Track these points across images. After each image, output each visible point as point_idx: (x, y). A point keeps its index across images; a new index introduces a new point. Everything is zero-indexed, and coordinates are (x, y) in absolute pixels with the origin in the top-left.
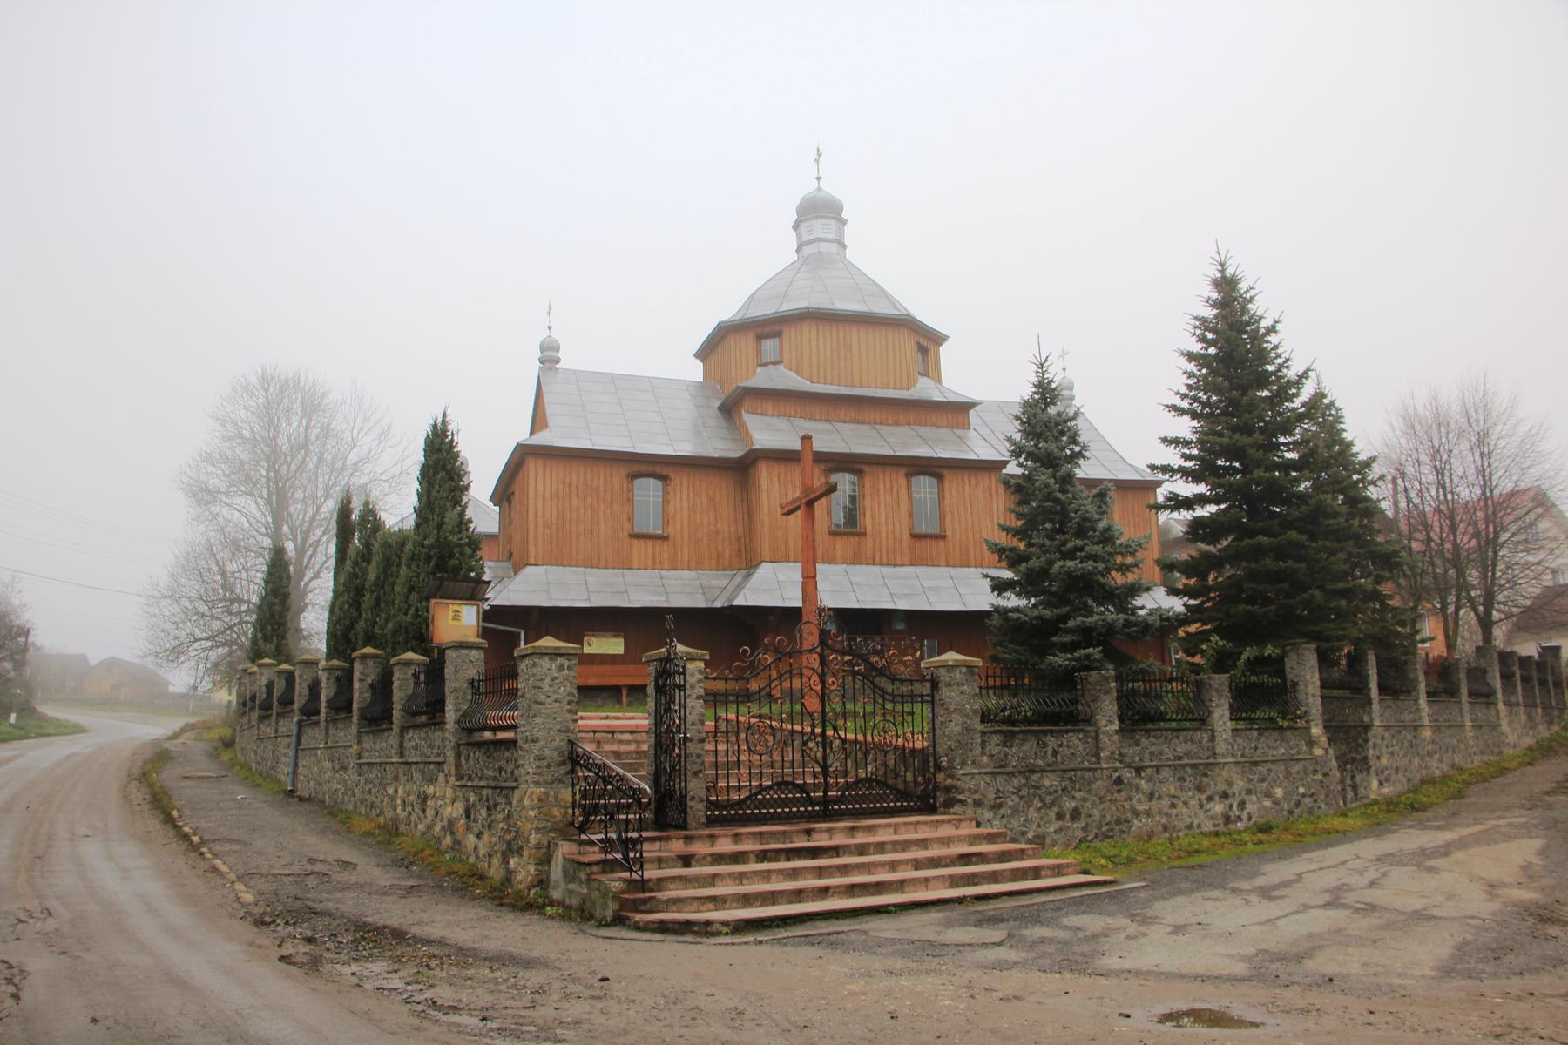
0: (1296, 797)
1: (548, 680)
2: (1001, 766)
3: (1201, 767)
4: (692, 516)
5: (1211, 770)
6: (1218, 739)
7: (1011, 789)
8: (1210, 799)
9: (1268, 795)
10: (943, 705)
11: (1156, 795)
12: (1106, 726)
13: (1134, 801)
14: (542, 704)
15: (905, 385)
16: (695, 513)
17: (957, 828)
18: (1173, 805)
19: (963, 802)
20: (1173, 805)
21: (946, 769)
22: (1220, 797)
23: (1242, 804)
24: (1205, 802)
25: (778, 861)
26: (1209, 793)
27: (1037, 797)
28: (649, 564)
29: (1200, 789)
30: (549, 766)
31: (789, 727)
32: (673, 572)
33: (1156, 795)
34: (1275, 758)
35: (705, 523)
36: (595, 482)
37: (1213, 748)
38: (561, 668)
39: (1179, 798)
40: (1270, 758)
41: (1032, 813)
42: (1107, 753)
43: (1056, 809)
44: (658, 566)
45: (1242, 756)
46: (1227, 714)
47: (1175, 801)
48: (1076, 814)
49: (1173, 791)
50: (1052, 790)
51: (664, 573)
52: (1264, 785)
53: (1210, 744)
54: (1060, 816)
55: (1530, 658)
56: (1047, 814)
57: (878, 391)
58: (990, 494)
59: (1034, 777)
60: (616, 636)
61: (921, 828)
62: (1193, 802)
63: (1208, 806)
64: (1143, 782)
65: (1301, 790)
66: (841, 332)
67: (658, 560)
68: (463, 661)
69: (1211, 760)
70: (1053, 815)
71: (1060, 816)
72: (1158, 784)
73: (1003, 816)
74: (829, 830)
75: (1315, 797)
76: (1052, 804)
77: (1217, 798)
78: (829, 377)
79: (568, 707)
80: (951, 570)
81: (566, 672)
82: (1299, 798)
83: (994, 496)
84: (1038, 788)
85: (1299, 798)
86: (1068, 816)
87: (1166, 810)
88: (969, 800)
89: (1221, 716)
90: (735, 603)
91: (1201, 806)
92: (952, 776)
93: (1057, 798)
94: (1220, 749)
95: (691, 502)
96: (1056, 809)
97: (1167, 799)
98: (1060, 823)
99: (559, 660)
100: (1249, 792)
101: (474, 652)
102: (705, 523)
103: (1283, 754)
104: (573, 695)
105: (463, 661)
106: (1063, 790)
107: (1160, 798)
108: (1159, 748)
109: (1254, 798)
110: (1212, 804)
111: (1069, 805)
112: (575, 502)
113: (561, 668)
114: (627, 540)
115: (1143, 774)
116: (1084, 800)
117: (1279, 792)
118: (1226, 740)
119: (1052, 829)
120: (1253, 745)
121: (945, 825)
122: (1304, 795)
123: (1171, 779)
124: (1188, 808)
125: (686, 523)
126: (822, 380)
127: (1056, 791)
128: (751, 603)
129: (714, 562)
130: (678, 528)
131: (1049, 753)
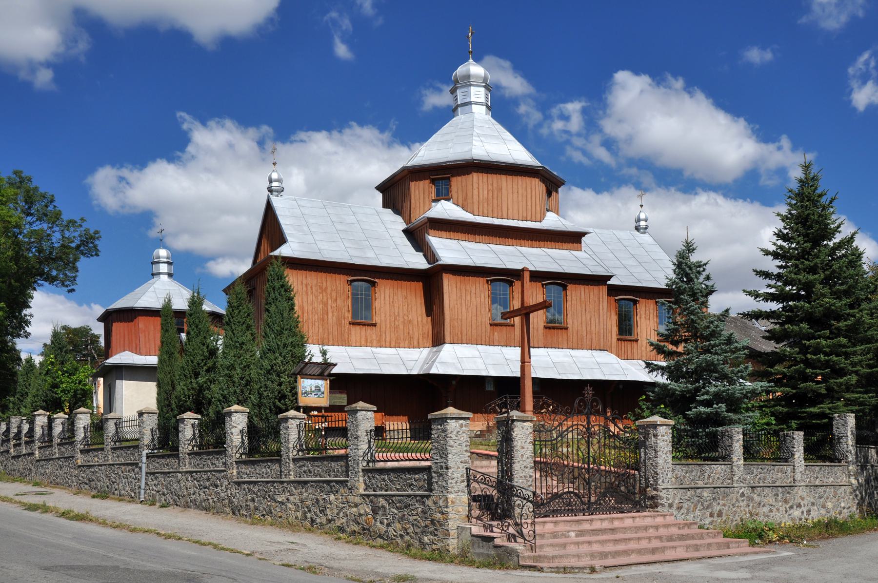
0: (839, 509)
1: (455, 433)
2: (682, 484)
3: (787, 488)
4: (392, 310)
5: (792, 490)
6: (797, 471)
7: (687, 498)
8: (791, 507)
9: (824, 507)
10: (652, 447)
11: (762, 504)
12: (737, 462)
13: (750, 507)
14: (452, 447)
15: (538, 219)
16: (394, 306)
17: (591, 524)
18: (771, 511)
19: (663, 505)
20: (771, 511)
21: (652, 485)
22: (797, 507)
23: (809, 511)
24: (788, 509)
25: (598, 535)
26: (791, 504)
27: (700, 503)
28: (363, 343)
29: (786, 501)
30: (456, 482)
31: (542, 459)
32: (379, 349)
33: (762, 504)
34: (828, 484)
35: (401, 314)
36: (324, 284)
37: (794, 476)
38: (461, 426)
39: (774, 506)
40: (825, 484)
41: (698, 512)
42: (737, 478)
43: (710, 511)
44: (368, 344)
45: (809, 482)
46: (802, 456)
47: (772, 508)
48: (720, 514)
49: (771, 502)
50: (708, 499)
51: (373, 349)
52: (822, 500)
53: (792, 474)
54: (712, 515)
55: (857, 381)
56: (705, 513)
57: (520, 222)
58: (599, 299)
59: (699, 491)
60: (341, 393)
61: (561, 524)
62: (782, 509)
63: (789, 512)
64: (755, 495)
65: (843, 505)
66: (481, 178)
67: (369, 340)
68: (363, 419)
69: (793, 484)
70: (708, 514)
71: (712, 515)
72: (763, 498)
73: (683, 514)
74: (556, 523)
75: (850, 509)
76: (708, 507)
77: (795, 507)
78: (486, 212)
79: (465, 449)
80: (571, 351)
81: (464, 428)
82: (841, 509)
83: (601, 300)
84: (701, 498)
85: (841, 509)
86: (716, 515)
87: (767, 513)
88: (666, 504)
89: (799, 457)
90: (431, 372)
91: (786, 512)
92: (656, 489)
93: (710, 504)
94: (798, 477)
95: (391, 300)
96: (710, 511)
97: (768, 506)
98: (712, 519)
99: (461, 422)
100: (813, 504)
101: (369, 413)
102: (401, 314)
103: (832, 482)
104: (468, 441)
105: (363, 419)
106: (713, 499)
107: (764, 506)
108: (764, 475)
109: (815, 508)
110: (792, 511)
111: (717, 508)
112: (311, 297)
113: (461, 426)
114: (348, 326)
115: (755, 491)
116: (724, 505)
117: (830, 505)
118: (801, 472)
119: (707, 522)
120: (815, 476)
121: (658, 517)
122: (844, 508)
123: (770, 494)
124: (779, 512)
125: (388, 314)
126: (481, 214)
127: (710, 500)
128: (441, 372)
129: (407, 342)
130: (383, 319)
131: (706, 477)
